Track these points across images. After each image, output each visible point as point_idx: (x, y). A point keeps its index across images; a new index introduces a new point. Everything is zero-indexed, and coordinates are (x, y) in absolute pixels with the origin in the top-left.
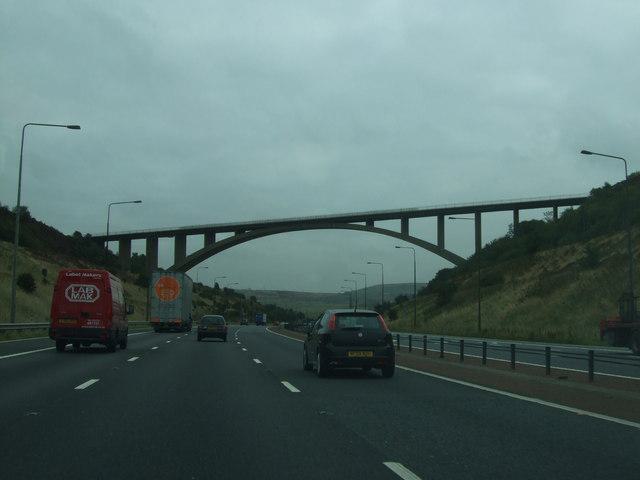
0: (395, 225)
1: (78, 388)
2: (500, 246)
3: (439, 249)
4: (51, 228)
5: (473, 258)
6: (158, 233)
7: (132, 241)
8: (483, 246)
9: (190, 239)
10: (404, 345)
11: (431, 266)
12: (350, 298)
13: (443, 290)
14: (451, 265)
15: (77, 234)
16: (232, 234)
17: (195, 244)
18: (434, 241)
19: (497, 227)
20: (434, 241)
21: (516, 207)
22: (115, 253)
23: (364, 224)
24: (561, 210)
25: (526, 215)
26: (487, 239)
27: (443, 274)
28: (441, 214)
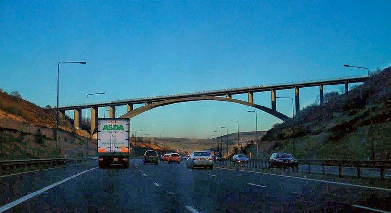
0: (245, 97)
1: (354, 205)
2: (313, 109)
3: (273, 111)
4: (32, 104)
5: (295, 117)
6: (81, 106)
7: (66, 111)
8: (301, 109)
9: (83, 111)
10: (31, 151)
11: (267, 123)
12: (218, 139)
13: (274, 137)
14: (281, 121)
15: (48, 106)
16: (361, 83)
17: (121, 111)
18: (270, 108)
19: (310, 98)
20: (270, 108)
21: (322, 84)
22: (271, 109)
23: (225, 96)
24: (351, 86)
25: (327, 90)
26: (303, 106)
27: (277, 128)
28: (274, 89)
